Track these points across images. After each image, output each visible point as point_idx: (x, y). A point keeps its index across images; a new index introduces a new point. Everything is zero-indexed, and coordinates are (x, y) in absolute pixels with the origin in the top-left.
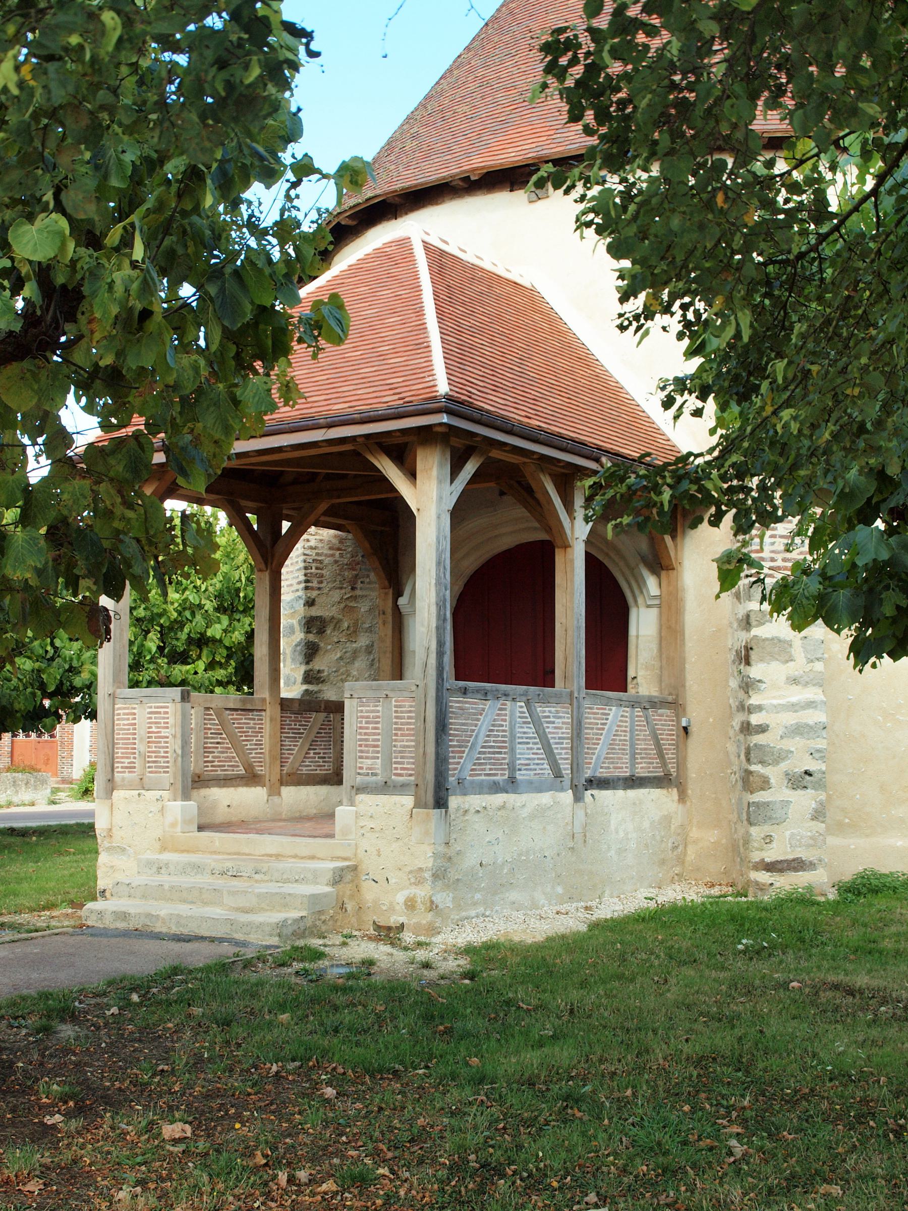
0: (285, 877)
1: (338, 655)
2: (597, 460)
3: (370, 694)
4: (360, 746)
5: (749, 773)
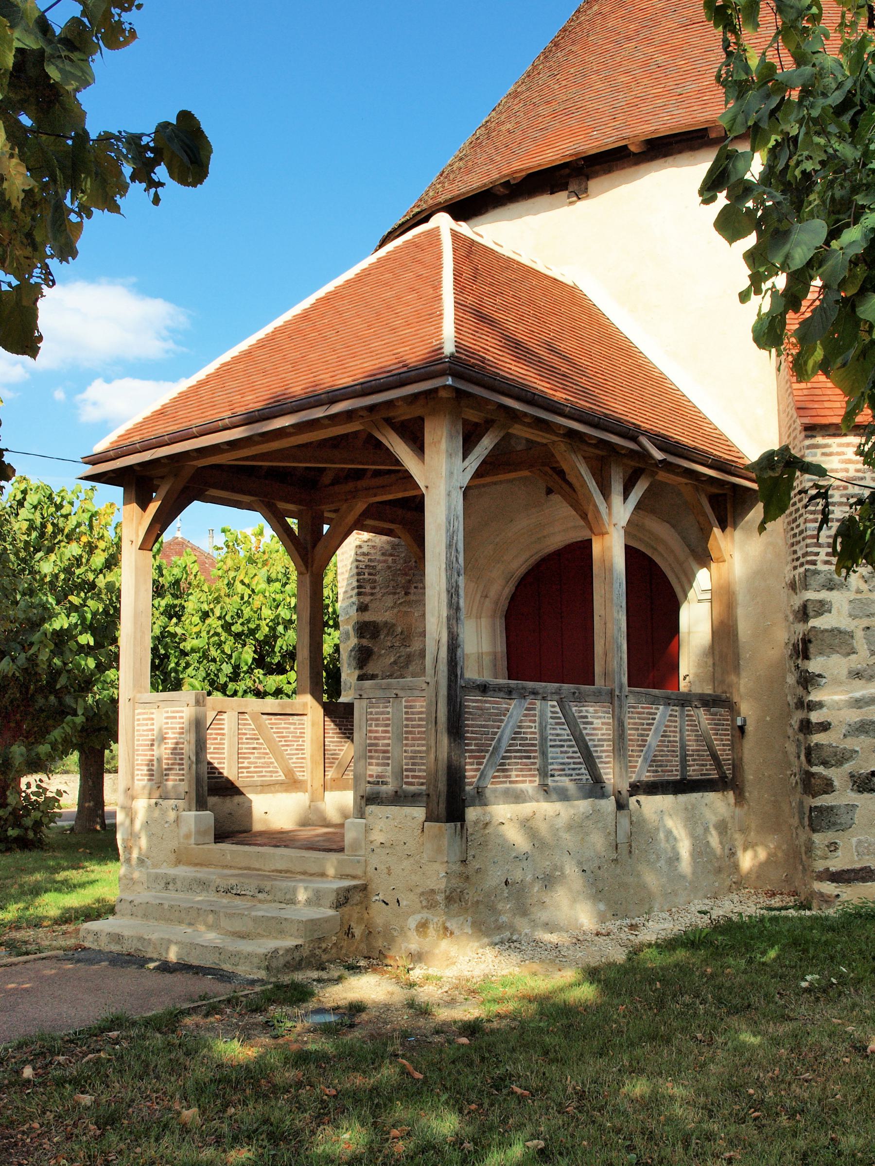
0: (288, 897)
1: (392, 660)
2: (634, 439)
3: (379, 694)
4: (370, 751)
5: (809, 775)
